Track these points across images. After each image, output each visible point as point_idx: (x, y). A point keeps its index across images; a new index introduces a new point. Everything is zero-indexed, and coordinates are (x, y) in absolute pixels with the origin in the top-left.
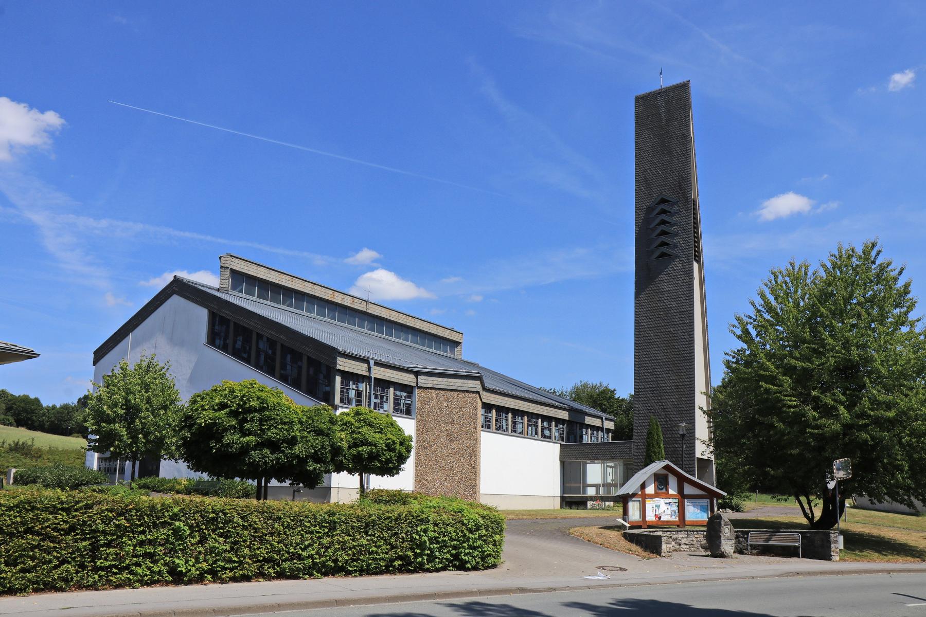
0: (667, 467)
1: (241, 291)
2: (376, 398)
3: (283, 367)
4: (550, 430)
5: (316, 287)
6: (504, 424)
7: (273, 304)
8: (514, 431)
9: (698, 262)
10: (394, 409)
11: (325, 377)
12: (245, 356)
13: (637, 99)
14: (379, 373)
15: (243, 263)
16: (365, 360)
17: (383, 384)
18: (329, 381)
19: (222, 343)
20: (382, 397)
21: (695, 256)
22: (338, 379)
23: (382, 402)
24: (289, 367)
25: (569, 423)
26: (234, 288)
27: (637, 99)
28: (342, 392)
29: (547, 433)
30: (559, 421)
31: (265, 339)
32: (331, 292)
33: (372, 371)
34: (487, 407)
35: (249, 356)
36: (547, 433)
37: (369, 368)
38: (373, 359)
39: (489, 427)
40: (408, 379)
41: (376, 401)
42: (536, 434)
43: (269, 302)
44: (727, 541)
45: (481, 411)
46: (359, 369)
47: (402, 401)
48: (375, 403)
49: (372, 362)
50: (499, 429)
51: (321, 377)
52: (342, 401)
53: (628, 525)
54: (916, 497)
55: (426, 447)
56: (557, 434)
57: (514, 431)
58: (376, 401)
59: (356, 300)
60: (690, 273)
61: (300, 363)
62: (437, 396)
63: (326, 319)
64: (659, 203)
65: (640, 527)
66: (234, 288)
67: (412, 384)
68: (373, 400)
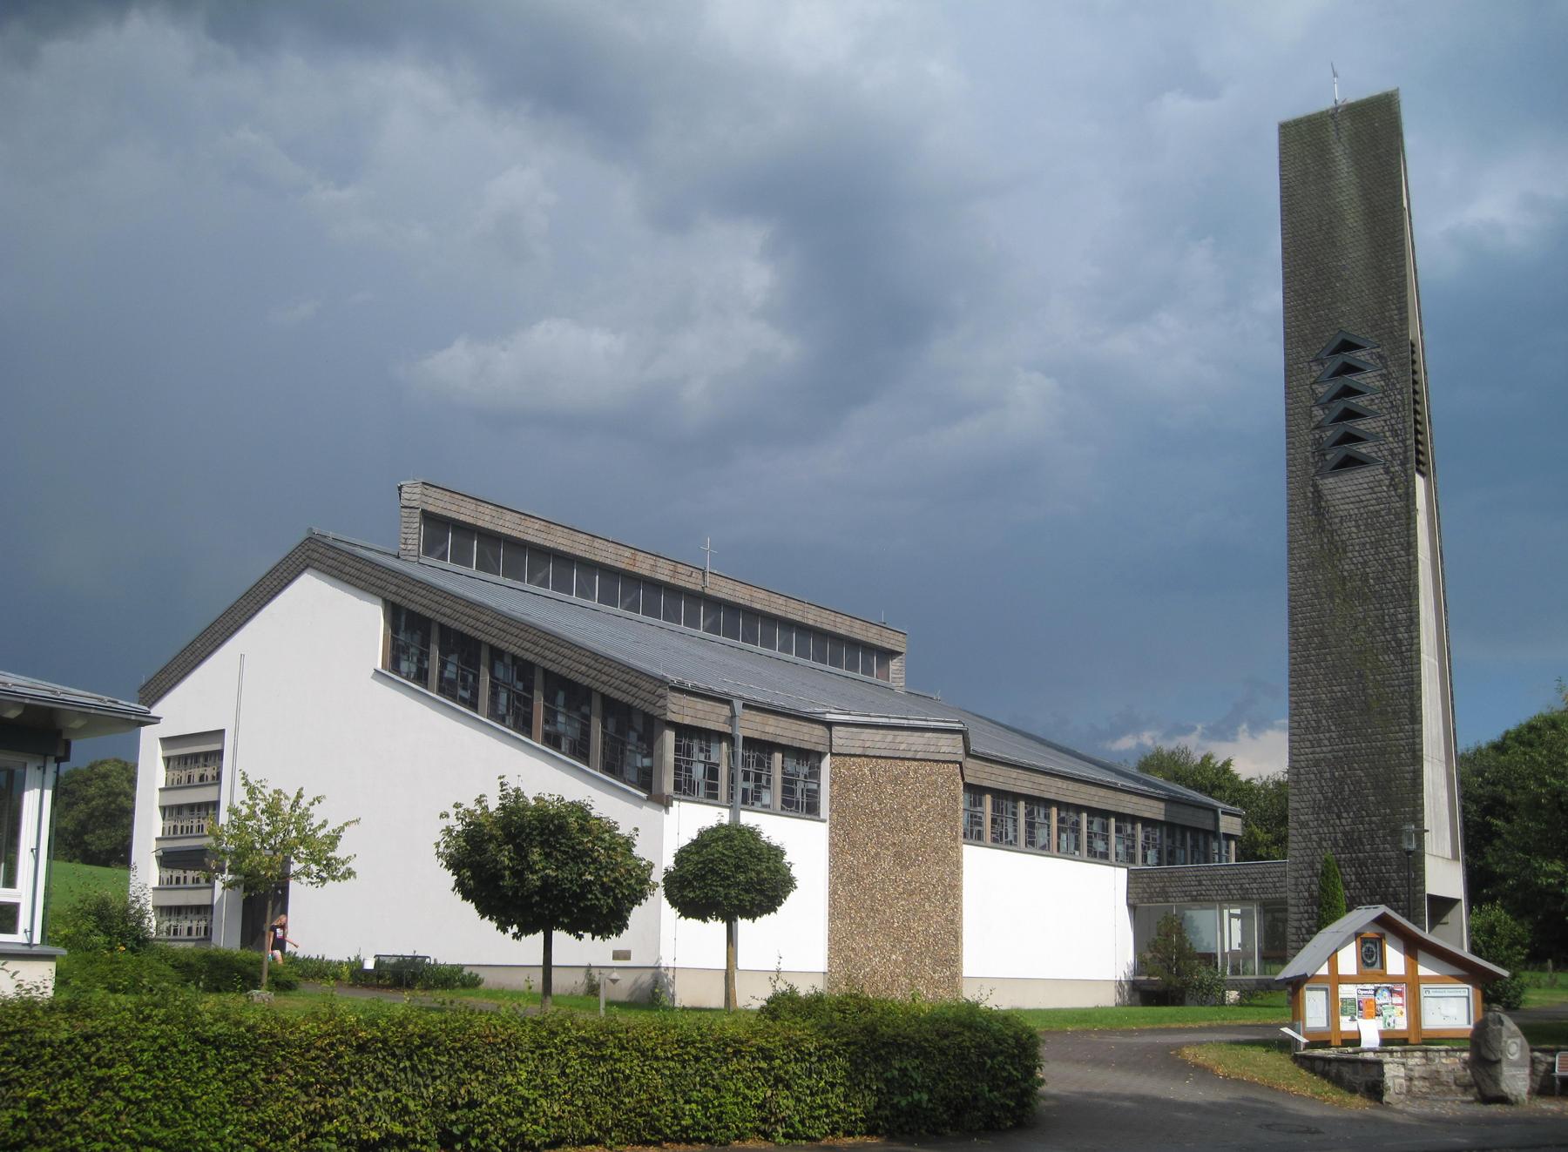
0: (1382, 921)
1: (443, 557)
2: (746, 778)
3: (550, 717)
4: (1106, 839)
5: (597, 543)
6: (1010, 830)
7: (508, 581)
8: (1031, 842)
9: (1423, 474)
10: (784, 801)
11: (640, 738)
12: (466, 695)
13: (1285, 128)
14: (751, 725)
15: (447, 496)
16: (725, 700)
17: (761, 748)
18: (651, 746)
19: (414, 669)
20: (758, 778)
21: (1418, 462)
22: (669, 737)
23: (758, 788)
24: (561, 719)
25: (1169, 827)
26: (428, 551)
27: (1285, 128)
28: (677, 768)
29: (1099, 846)
30: (1147, 822)
31: (508, 660)
32: (628, 553)
33: (738, 722)
34: (975, 791)
35: (475, 694)
36: (1099, 846)
37: (733, 717)
38: (740, 698)
39: (979, 836)
40: (807, 736)
41: (745, 785)
42: (1077, 847)
43: (500, 579)
44: (1513, 1071)
45: (962, 799)
46: (711, 717)
47: (800, 785)
48: (745, 791)
49: (738, 704)
50: (1001, 840)
51: (633, 736)
52: (677, 786)
53: (1303, 1040)
54: (1493, 815)
55: (851, 881)
56: (1121, 848)
57: (1031, 842)
58: (745, 785)
59: (680, 568)
60: (1410, 496)
61: (585, 709)
62: (872, 772)
63: (618, 610)
64: (1337, 351)
65: (1326, 1044)
66: (428, 551)
67: (820, 748)
68: (741, 784)
